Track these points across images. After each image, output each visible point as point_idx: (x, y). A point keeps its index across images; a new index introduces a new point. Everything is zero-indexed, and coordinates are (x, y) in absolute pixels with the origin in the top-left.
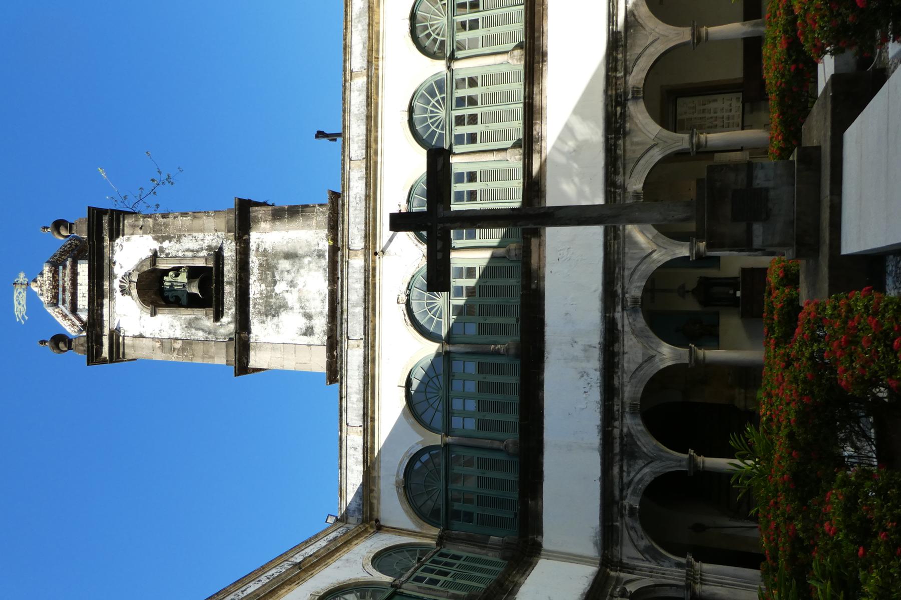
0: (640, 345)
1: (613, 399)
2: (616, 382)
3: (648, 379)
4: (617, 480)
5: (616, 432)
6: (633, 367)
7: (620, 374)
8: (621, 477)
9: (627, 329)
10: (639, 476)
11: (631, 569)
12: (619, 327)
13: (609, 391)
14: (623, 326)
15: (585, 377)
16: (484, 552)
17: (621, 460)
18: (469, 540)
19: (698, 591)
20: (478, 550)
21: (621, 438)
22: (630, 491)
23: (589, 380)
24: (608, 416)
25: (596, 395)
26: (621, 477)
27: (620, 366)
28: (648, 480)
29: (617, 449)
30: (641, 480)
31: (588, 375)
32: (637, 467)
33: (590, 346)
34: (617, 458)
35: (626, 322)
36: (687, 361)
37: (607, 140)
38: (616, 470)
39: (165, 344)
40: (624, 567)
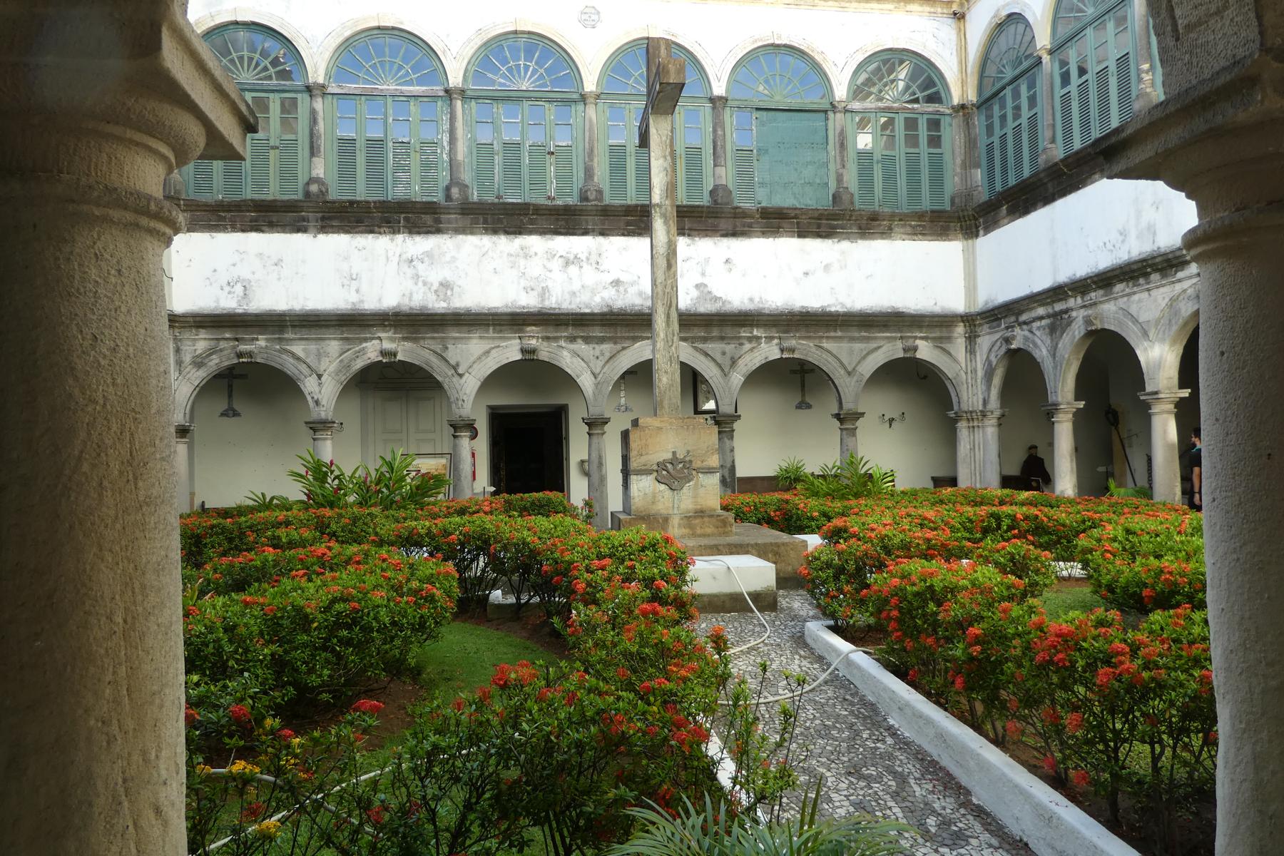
0: (1157, 314)
1: (1100, 288)
2: (1119, 287)
3: (1124, 335)
4: (1034, 314)
5: (1071, 303)
6: (1133, 310)
7: (1128, 290)
8: (1034, 320)
9: (1178, 287)
10: (1039, 342)
11: (971, 351)
12: (1180, 275)
13: (1106, 280)
14: (1179, 281)
15: (1121, 238)
16: (958, 170)
17: (1049, 316)
18: (971, 143)
19: (959, 424)
20: (959, 161)
21: (1066, 311)
22: (1026, 333)
23: (1117, 246)
24: (1081, 286)
25: (1104, 261)
26: (1034, 320)
27: (1135, 289)
28: (1036, 354)
29: (1059, 307)
30: (1035, 345)
31: (1123, 241)
32: (1044, 338)
33: (1155, 234)
34: (1050, 311)
35: (1186, 284)
36: (1149, 388)
37: (1039, 294)
38: (1041, 311)
39: (666, 223)
40: (971, 338)
